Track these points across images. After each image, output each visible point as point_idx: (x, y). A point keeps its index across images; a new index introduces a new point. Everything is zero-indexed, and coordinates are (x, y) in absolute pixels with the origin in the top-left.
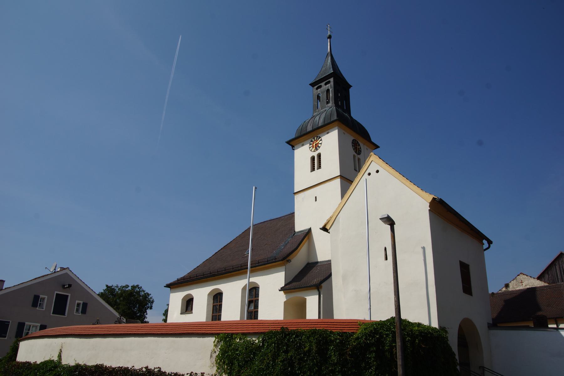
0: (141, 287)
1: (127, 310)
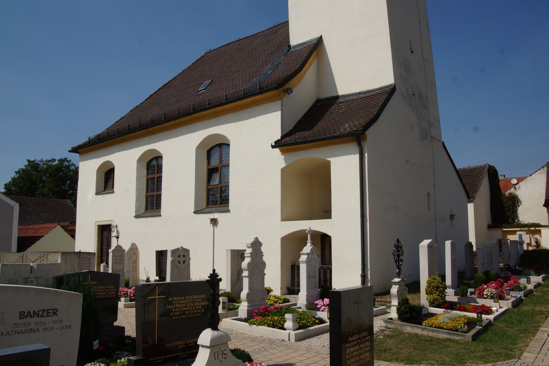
0: (70, 160)
1: (54, 188)
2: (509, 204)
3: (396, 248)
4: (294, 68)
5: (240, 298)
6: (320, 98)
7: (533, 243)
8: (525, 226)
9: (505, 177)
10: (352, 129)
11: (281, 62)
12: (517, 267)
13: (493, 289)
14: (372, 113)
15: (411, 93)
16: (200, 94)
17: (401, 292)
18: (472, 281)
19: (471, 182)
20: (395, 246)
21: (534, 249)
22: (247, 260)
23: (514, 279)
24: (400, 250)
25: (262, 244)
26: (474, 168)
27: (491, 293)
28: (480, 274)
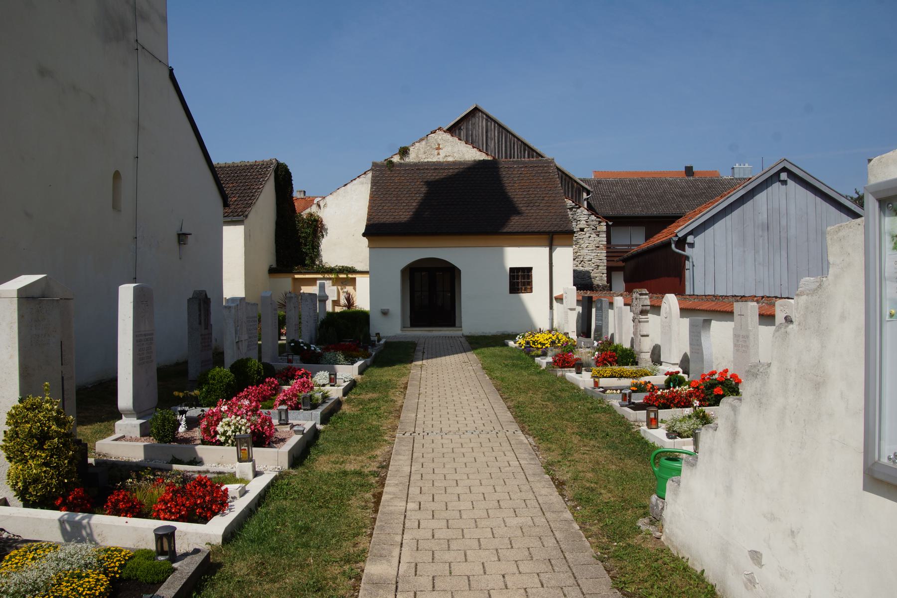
2: (306, 232)
7: (343, 301)
8: (331, 270)
9: (305, 195)
12: (312, 346)
19: (243, 188)
21: (344, 311)
26: (251, 165)
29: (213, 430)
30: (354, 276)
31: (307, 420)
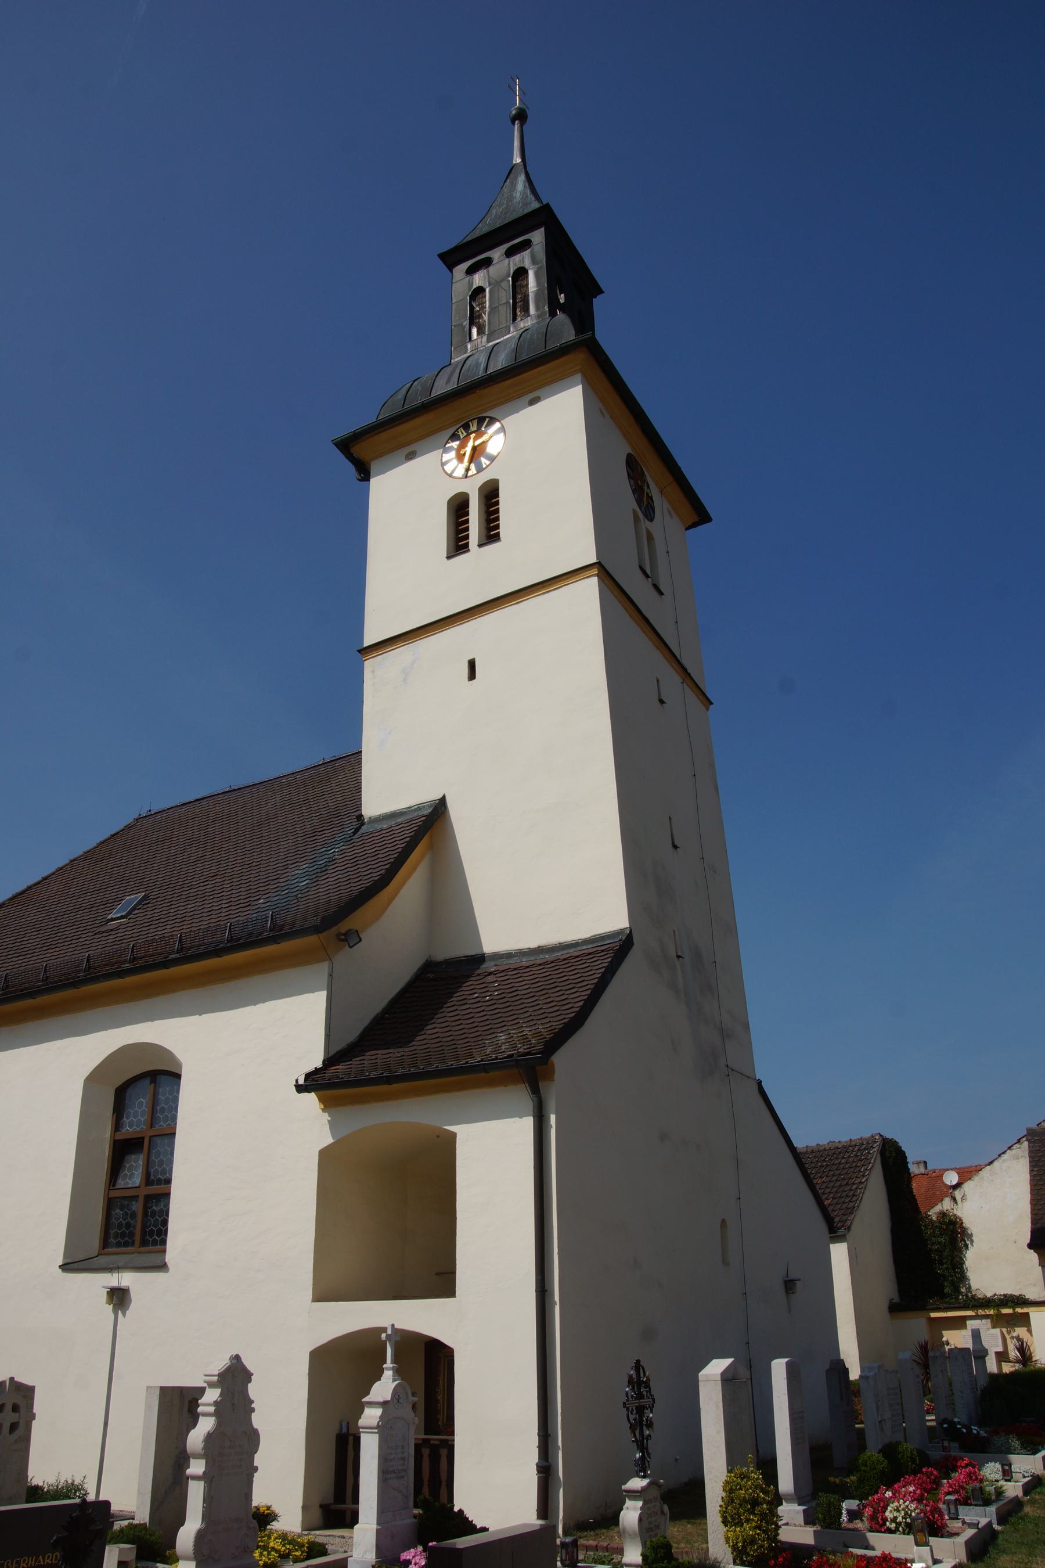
2: (940, 1243)
3: (633, 1389)
4: (370, 876)
5: (174, 1546)
6: (433, 959)
7: (1013, 1353)
9: (926, 1168)
10: (514, 1047)
11: (335, 860)
12: (973, 1427)
13: (911, 1502)
14: (570, 1006)
15: (672, 953)
16: (111, 930)
17: (650, 1520)
18: (852, 1478)
19: (838, 1184)
20: (630, 1382)
21: (1016, 1370)
22: (205, 1425)
23: (967, 1465)
24: (645, 1393)
25: (252, 1374)
27: (906, 1513)
28: (872, 1456)
29: (880, 1517)
30: (1025, 1310)
31: (984, 1516)
